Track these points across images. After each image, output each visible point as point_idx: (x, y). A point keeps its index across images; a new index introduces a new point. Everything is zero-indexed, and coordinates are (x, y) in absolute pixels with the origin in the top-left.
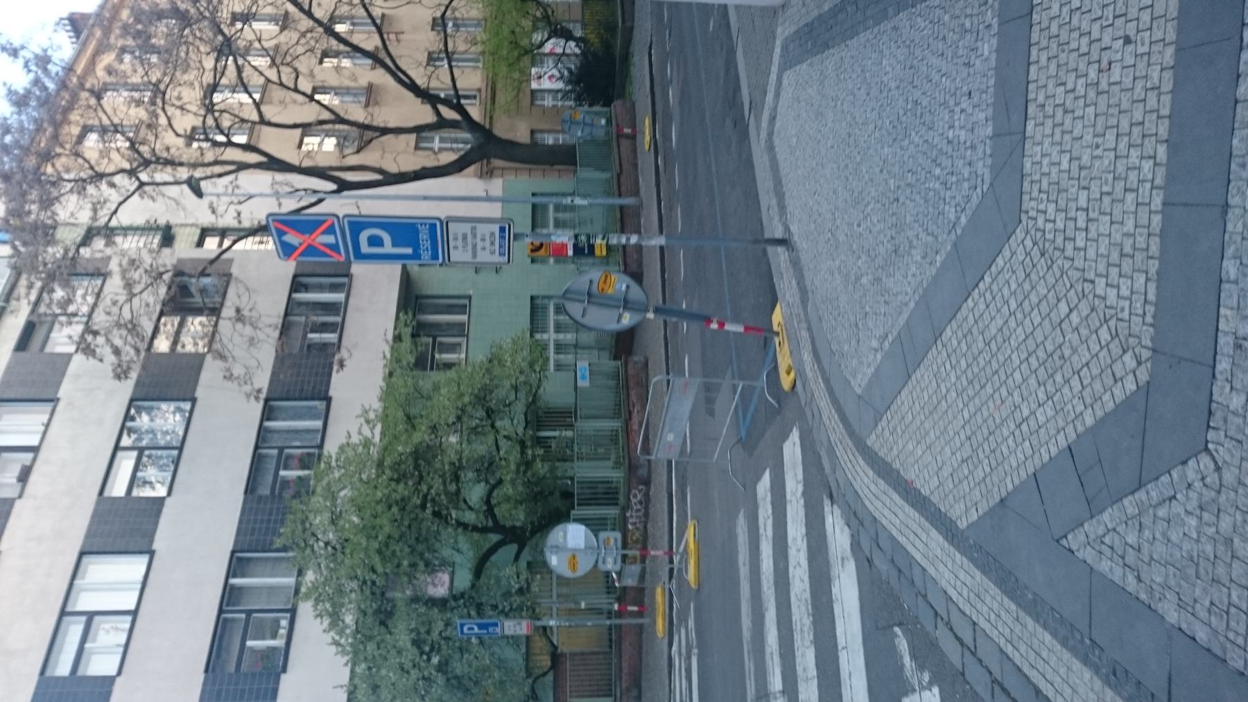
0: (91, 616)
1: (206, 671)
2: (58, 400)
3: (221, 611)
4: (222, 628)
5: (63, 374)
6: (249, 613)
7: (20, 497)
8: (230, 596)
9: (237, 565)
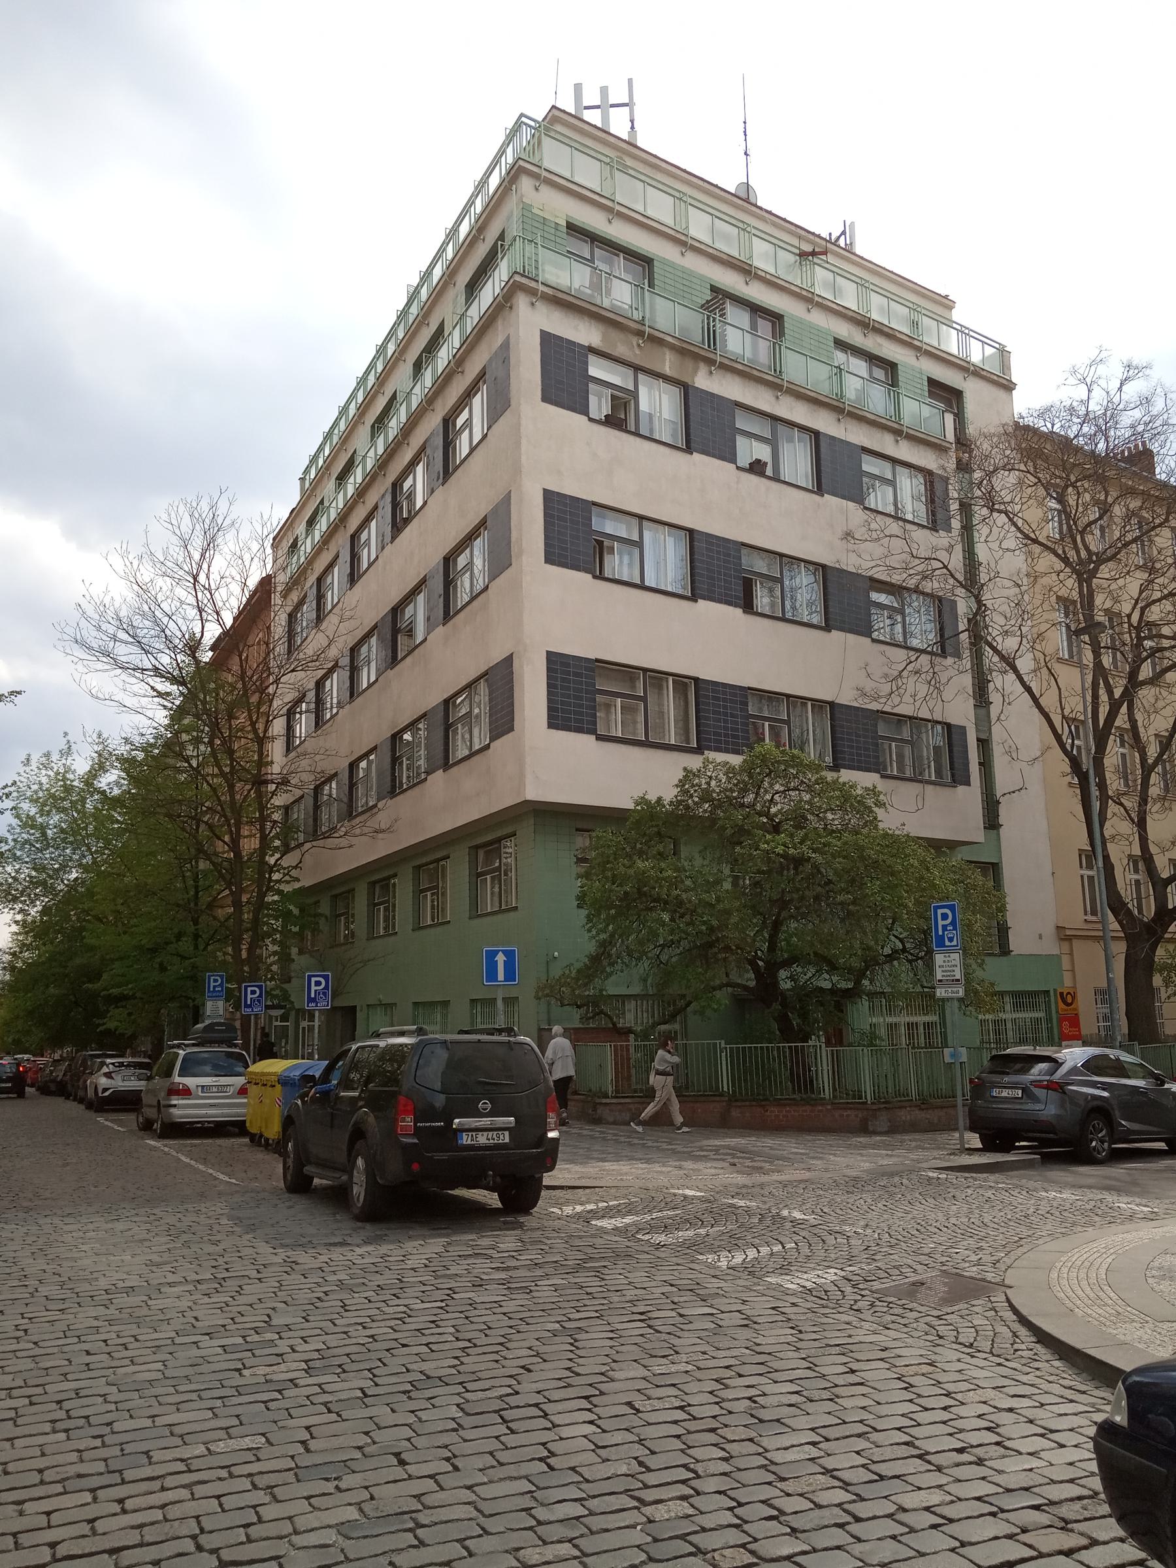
0: (639, 544)
1: (597, 660)
2: (937, 531)
3: (645, 670)
4: (627, 672)
5: (843, 497)
6: (644, 699)
7: (591, 420)
8: (656, 677)
9: (683, 683)
